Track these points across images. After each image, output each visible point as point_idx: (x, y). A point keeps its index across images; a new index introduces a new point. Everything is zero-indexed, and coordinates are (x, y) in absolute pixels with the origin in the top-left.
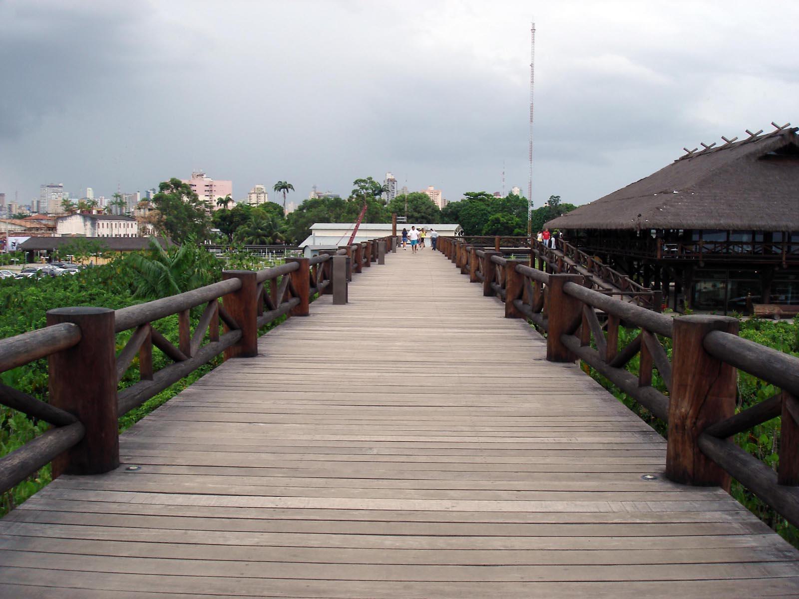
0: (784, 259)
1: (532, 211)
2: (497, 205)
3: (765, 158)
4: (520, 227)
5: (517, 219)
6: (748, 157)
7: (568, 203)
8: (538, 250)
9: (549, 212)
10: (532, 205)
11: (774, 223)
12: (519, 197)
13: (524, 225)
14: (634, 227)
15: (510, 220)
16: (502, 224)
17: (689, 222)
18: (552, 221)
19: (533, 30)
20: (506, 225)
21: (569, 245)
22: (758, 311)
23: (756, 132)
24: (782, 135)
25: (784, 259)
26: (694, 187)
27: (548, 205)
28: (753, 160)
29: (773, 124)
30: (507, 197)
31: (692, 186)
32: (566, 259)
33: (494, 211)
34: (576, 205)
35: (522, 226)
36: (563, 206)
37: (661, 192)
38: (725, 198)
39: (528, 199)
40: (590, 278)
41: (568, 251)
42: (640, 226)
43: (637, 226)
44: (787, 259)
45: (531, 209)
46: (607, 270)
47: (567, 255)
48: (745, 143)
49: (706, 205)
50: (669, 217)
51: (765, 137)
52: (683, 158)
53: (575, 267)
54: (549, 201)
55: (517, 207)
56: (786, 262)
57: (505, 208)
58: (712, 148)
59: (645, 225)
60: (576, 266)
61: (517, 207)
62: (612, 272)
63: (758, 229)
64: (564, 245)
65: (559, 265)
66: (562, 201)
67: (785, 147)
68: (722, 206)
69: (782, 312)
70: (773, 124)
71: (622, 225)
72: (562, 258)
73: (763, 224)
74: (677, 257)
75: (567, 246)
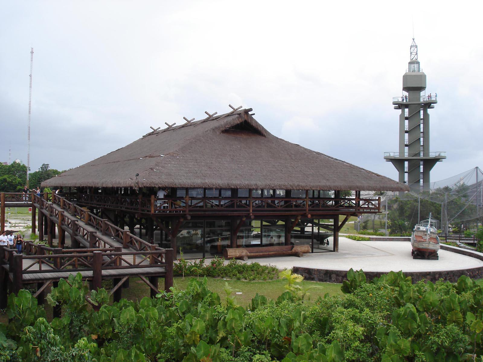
0: (251, 211)
1: (30, 174)
2: (5, 169)
3: (226, 131)
4: (21, 185)
5: (19, 179)
6: (214, 130)
7: (54, 169)
8: (39, 204)
9: (42, 174)
10: (30, 170)
11: (246, 183)
12: (20, 164)
13: (24, 183)
14: (133, 185)
15: (14, 180)
16: (9, 183)
17: (180, 181)
18: (48, 181)
19: (32, 52)
20: (11, 183)
21: (66, 200)
22: (231, 254)
23: (191, 119)
24: (239, 114)
25: (251, 211)
26: (177, 152)
27: (40, 170)
28: (218, 133)
29: (230, 106)
30: (12, 164)
31: (176, 151)
32: (66, 213)
33: (3, 174)
34: (60, 170)
35: (23, 184)
36: (51, 171)
37: (146, 157)
38: (204, 162)
39: (26, 165)
40: (94, 234)
41: (65, 205)
42: (138, 185)
43: (136, 185)
44: (253, 211)
45: (28, 172)
46: (106, 224)
47: (67, 211)
48: (204, 121)
49: (191, 166)
50: (163, 177)
51: (224, 116)
52: (150, 134)
53: (76, 222)
54: (41, 168)
55: (18, 171)
56: (253, 214)
57: (10, 172)
58: (173, 126)
59: (143, 184)
60: (77, 221)
61: (18, 171)
62: (111, 226)
63: (236, 187)
64: (61, 200)
65: (60, 218)
66: (51, 168)
67: (241, 123)
68: (203, 167)
69: (249, 254)
70: (230, 106)
71: (119, 183)
72: (62, 213)
73: (239, 183)
74: (168, 212)
75: (64, 201)
